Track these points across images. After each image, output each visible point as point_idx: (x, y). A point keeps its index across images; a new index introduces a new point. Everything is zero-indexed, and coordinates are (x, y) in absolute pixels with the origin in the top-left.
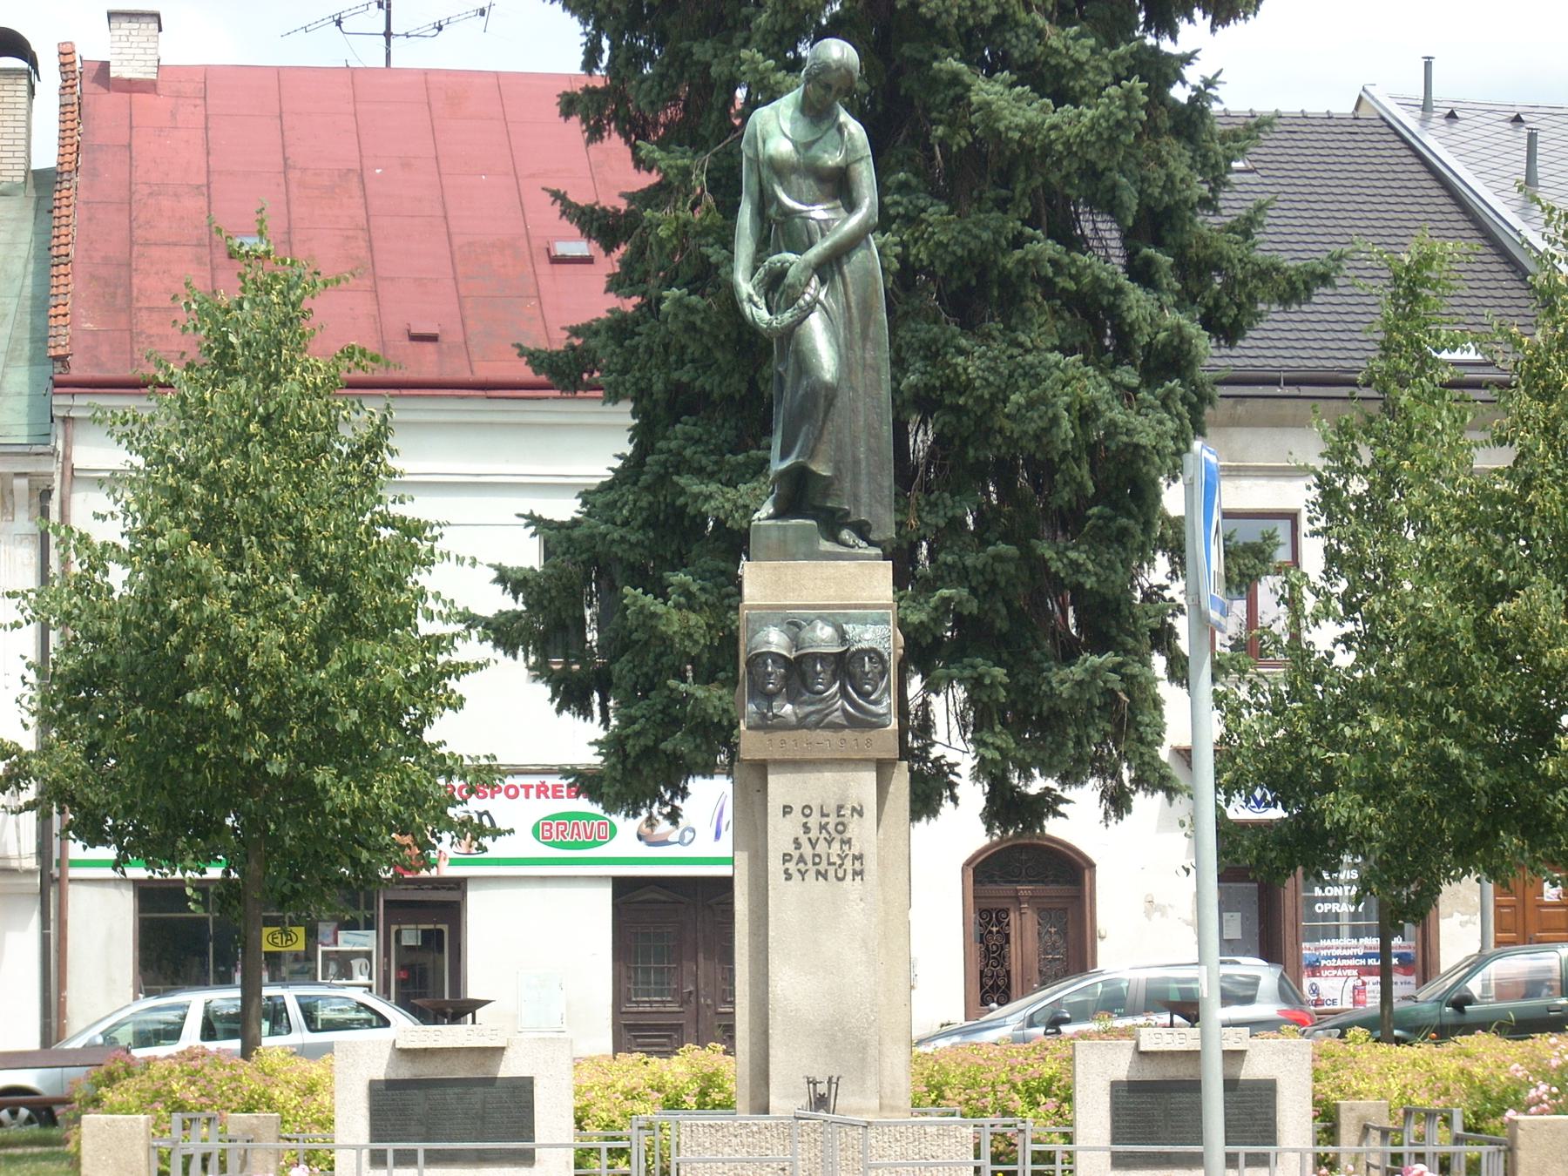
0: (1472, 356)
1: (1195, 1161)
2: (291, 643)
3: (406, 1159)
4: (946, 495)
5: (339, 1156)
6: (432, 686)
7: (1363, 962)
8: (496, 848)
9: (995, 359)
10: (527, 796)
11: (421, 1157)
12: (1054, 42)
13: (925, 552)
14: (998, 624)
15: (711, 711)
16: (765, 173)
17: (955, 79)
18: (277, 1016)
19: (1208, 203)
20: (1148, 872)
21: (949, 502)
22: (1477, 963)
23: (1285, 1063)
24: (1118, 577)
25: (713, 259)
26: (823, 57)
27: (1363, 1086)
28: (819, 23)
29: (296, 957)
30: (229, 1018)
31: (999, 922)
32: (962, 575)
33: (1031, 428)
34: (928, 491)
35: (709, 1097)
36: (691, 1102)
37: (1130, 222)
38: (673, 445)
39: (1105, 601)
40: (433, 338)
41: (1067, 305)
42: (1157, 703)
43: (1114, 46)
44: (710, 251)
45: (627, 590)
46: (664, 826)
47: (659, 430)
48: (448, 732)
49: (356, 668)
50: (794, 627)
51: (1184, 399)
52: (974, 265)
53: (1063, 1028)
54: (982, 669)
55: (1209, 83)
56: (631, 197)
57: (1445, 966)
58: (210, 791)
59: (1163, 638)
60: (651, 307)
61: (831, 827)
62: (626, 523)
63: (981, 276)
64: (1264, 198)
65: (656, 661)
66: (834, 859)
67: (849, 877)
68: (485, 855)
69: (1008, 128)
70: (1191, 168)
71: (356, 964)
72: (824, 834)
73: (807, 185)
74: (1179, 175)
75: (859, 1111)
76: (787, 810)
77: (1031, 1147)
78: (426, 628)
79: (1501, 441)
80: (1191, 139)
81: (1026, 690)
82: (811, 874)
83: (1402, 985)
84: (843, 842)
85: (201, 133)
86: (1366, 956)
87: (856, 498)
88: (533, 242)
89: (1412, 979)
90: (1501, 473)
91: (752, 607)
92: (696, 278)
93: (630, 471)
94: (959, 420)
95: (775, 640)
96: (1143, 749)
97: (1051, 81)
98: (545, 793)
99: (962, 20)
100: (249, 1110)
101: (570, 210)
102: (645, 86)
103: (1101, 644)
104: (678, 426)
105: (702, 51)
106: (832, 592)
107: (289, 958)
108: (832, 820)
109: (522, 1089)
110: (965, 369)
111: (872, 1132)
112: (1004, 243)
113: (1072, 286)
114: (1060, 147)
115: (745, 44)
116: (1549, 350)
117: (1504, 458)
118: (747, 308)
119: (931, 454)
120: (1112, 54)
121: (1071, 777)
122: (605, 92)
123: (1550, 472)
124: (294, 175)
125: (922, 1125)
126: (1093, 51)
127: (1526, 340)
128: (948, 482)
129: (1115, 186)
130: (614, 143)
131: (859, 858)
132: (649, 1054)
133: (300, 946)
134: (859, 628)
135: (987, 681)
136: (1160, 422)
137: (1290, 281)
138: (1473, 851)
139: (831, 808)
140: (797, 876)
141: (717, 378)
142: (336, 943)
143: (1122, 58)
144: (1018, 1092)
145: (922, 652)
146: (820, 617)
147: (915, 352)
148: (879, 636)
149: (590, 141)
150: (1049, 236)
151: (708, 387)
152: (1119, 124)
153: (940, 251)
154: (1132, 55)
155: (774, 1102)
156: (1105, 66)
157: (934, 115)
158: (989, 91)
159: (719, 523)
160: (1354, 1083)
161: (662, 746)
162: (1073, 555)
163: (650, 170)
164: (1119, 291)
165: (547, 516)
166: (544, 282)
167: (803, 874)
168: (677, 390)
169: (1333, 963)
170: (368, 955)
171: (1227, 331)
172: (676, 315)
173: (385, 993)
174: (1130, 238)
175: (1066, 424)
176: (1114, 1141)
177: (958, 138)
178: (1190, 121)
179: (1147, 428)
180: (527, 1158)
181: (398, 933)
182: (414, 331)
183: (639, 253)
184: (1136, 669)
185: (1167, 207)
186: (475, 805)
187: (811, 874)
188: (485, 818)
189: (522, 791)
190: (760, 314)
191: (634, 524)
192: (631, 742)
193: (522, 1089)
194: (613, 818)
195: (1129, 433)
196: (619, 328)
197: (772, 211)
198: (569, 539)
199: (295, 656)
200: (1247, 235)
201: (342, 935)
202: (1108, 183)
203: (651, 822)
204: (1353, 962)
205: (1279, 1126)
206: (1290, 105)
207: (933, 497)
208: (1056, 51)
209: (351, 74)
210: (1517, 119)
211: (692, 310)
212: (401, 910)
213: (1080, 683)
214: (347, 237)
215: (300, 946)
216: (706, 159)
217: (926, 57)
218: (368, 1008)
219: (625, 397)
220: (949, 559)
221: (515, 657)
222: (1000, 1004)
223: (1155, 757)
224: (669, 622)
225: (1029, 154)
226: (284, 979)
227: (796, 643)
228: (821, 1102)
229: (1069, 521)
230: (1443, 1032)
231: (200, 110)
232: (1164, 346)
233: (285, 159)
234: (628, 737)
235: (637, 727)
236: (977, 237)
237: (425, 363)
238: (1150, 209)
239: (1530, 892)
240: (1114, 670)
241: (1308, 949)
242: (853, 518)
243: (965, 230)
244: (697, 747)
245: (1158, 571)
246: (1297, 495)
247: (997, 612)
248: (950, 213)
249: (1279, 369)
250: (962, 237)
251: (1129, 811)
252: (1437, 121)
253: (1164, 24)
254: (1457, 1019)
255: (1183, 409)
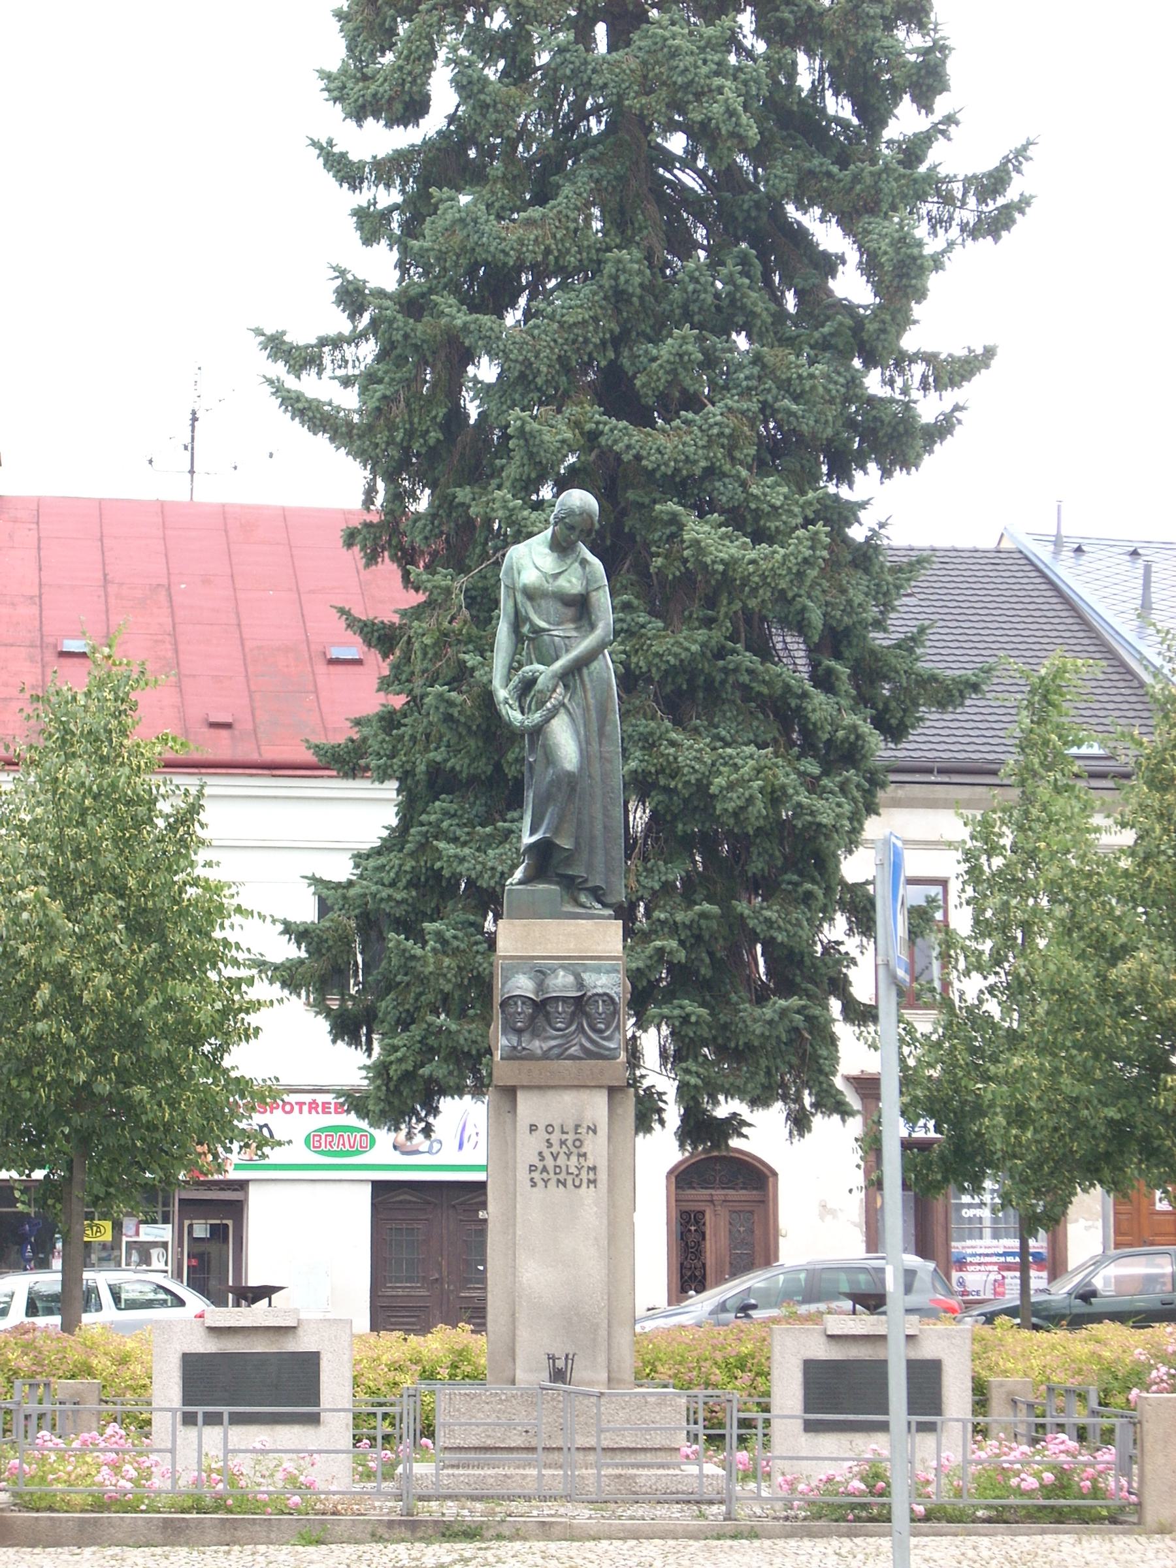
0: (1096, 750)
1: (884, 1427)
2: (116, 984)
3: (213, 1420)
4: (661, 863)
5: (156, 1418)
6: (230, 1022)
7: (1002, 1259)
8: (275, 1155)
9: (700, 750)
10: (301, 1112)
11: (226, 1418)
12: (754, 490)
13: (642, 909)
14: (703, 971)
15: (462, 1041)
16: (519, 597)
17: (674, 520)
18: (90, 1300)
19: (879, 625)
20: (820, 1182)
21: (663, 869)
22: (1097, 1263)
23: (951, 1346)
24: (804, 933)
25: (469, 664)
26: (569, 504)
27: (1010, 1365)
28: (558, 473)
29: (104, 1246)
30: (54, 1298)
31: (697, 1222)
32: (674, 929)
33: (731, 806)
34: (646, 859)
35: (461, 1370)
36: (444, 1373)
37: (816, 639)
38: (433, 818)
39: (791, 952)
40: (227, 726)
41: (762, 708)
42: (832, 1040)
43: (803, 493)
44: (467, 657)
45: (392, 935)
46: (419, 1138)
47: (419, 805)
48: (242, 1060)
49: (168, 1004)
50: (541, 975)
51: (858, 786)
52: (685, 672)
53: (754, 1314)
54: (689, 1009)
55: (882, 525)
56: (404, 614)
57: (1072, 1264)
58: (44, 1107)
59: (840, 986)
60: (416, 702)
61: (569, 1143)
62: (393, 884)
63: (690, 682)
64: (927, 623)
65: (416, 1000)
66: (573, 1170)
67: (584, 1185)
68: (266, 1161)
69: (714, 562)
70: (867, 595)
71: (155, 1253)
72: (564, 1148)
73: (552, 607)
74: (857, 601)
75: (591, 1383)
76: (533, 1128)
77: (736, 1415)
78: (230, 972)
79: (1124, 825)
80: (867, 571)
81: (725, 1027)
82: (553, 1183)
83: (1038, 1279)
84: (579, 1155)
85: (34, 552)
86: (1005, 1254)
87: (590, 867)
88: (313, 647)
89: (1044, 1274)
90: (1122, 851)
91: (505, 958)
92: (454, 680)
93: (396, 839)
94: (671, 799)
95: (523, 985)
96: (822, 1078)
97: (750, 523)
98: (316, 1109)
99: (677, 470)
100: (73, 1377)
101: (353, 623)
102: (420, 524)
103: (786, 988)
104: (437, 803)
105: (463, 494)
106: (572, 946)
107: (97, 1248)
108: (570, 1137)
109: (311, 1361)
110: (676, 759)
111: (603, 1400)
112: (709, 654)
113: (765, 690)
114: (756, 579)
115: (499, 487)
116: (1165, 750)
117: (1128, 837)
118: (504, 710)
119: (648, 828)
120: (802, 500)
121: (759, 1101)
122: (380, 525)
123: (1164, 852)
124: (112, 589)
125: (644, 1395)
126: (786, 498)
127: (1145, 739)
128: (662, 853)
129: (804, 609)
130: (388, 568)
131: (594, 1169)
132: (408, 1332)
133: (108, 1237)
134: (594, 976)
135: (693, 1019)
136: (839, 805)
137: (948, 690)
138: (1099, 1166)
139: (570, 1127)
140: (541, 1184)
141: (467, 761)
142: (137, 1234)
143: (810, 504)
144: (719, 1368)
145: (643, 998)
146: (562, 967)
147: (635, 743)
148: (608, 982)
149: (367, 565)
150: (748, 648)
151: (458, 768)
152: (806, 561)
153: (657, 660)
154: (819, 500)
155: (520, 1375)
156: (796, 510)
157: (654, 549)
158: (697, 529)
159: (471, 883)
160: (1001, 1362)
161: (421, 1071)
162: (768, 913)
163: (417, 590)
164: (805, 695)
165: (326, 878)
166: (322, 680)
167: (546, 1182)
168: (435, 770)
169: (977, 1260)
170: (164, 1245)
171: (895, 732)
172: (437, 708)
173: (179, 1276)
174: (813, 651)
175: (759, 804)
176: (807, 1410)
177: (673, 569)
178: (865, 556)
179: (827, 810)
180: (313, 1420)
181: (191, 1226)
182: (211, 720)
183: (407, 658)
184: (817, 1011)
185: (847, 628)
186: (258, 1119)
187: (553, 1183)
188: (265, 1131)
189: (296, 1108)
190: (515, 716)
191: (401, 885)
192: (394, 1067)
193: (311, 1361)
194: (375, 1132)
195: (812, 813)
196: (389, 721)
197: (525, 629)
198: (344, 897)
199: (119, 994)
200: (911, 650)
201: (143, 1227)
202: (799, 607)
203: (410, 1137)
204: (994, 1259)
205: (944, 1399)
206: (943, 541)
207: (649, 865)
208: (756, 497)
209: (162, 507)
210: (1135, 553)
211: (451, 703)
212: (192, 1208)
213: (770, 1022)
214: (156, 641)
215: (108, 1237)
216: (463, 580)
217: (647, 500)
218: (167, 1291)
219: (390, 777)
220: (662, 916)
221: (299, 995)
222: (698, 1292)
223: (832, 1086)
224: (425, 964)
225: (727, 582)
226: (93, 1265)
227: (540, 986)
228: (558, 1375)
229: (765, 886)
230: (1077, 1321)
231: (35, 533)
232: (842, 742)
233: (105, 575)
234: (391, 1063)
235: (399, 1054)
236: (687, 649)
237: (221, 747)
238: (832, 629)
239: (1145, 1201)
240: (798, 1012)
241: (957, 1247)
242: (590, 884)
243: (677, 643)
244: (451, 1073)
245: (837, 929)
246: (950, 865)
247: (702, 960)
248: (665, 629)
249: (934, 760)
250: (675, 649)
251: (809, 1130)
252: (1067, 554)
253: (842, 473)
254: (1084, 1311)
255: (857, 794)
